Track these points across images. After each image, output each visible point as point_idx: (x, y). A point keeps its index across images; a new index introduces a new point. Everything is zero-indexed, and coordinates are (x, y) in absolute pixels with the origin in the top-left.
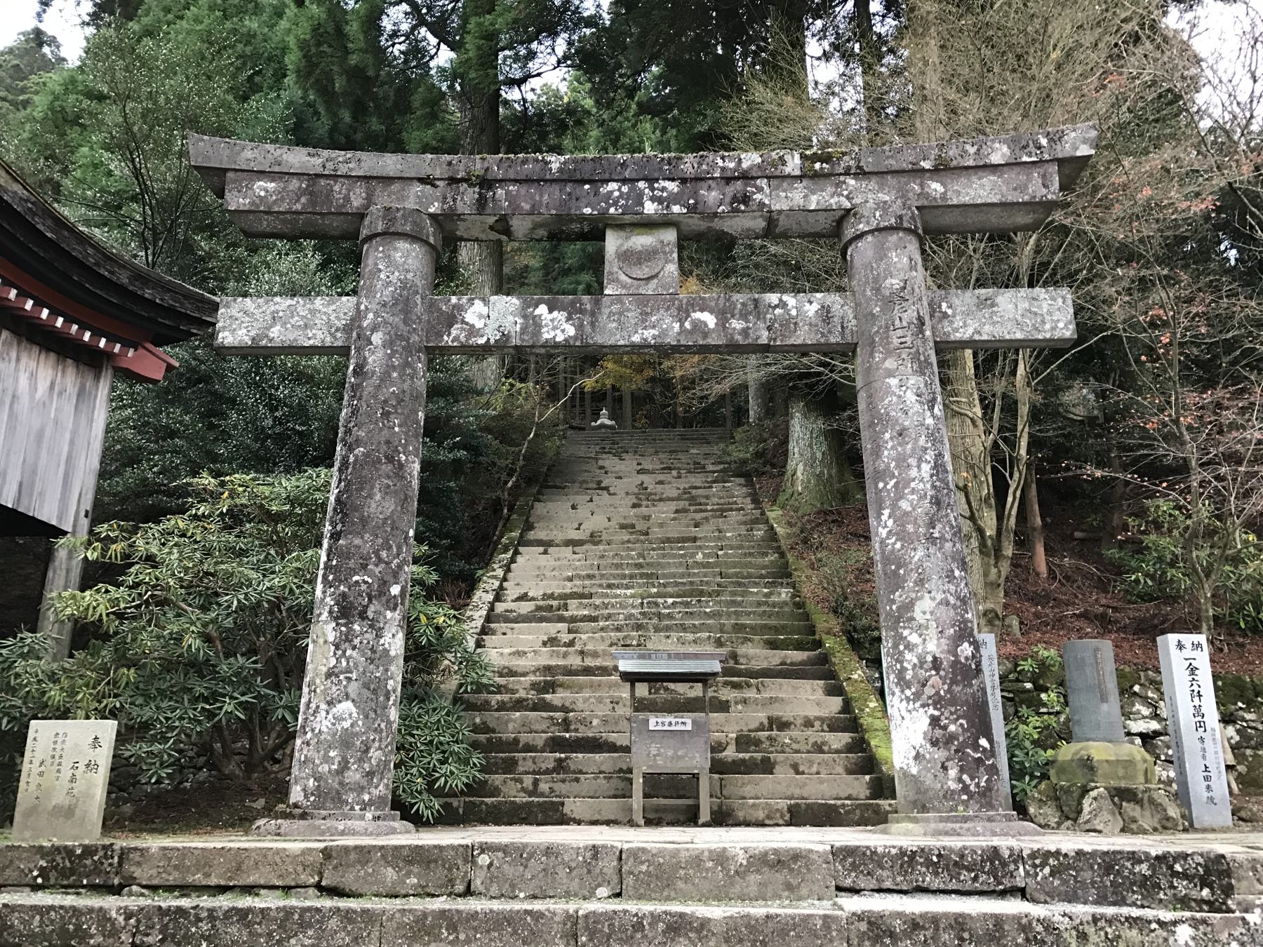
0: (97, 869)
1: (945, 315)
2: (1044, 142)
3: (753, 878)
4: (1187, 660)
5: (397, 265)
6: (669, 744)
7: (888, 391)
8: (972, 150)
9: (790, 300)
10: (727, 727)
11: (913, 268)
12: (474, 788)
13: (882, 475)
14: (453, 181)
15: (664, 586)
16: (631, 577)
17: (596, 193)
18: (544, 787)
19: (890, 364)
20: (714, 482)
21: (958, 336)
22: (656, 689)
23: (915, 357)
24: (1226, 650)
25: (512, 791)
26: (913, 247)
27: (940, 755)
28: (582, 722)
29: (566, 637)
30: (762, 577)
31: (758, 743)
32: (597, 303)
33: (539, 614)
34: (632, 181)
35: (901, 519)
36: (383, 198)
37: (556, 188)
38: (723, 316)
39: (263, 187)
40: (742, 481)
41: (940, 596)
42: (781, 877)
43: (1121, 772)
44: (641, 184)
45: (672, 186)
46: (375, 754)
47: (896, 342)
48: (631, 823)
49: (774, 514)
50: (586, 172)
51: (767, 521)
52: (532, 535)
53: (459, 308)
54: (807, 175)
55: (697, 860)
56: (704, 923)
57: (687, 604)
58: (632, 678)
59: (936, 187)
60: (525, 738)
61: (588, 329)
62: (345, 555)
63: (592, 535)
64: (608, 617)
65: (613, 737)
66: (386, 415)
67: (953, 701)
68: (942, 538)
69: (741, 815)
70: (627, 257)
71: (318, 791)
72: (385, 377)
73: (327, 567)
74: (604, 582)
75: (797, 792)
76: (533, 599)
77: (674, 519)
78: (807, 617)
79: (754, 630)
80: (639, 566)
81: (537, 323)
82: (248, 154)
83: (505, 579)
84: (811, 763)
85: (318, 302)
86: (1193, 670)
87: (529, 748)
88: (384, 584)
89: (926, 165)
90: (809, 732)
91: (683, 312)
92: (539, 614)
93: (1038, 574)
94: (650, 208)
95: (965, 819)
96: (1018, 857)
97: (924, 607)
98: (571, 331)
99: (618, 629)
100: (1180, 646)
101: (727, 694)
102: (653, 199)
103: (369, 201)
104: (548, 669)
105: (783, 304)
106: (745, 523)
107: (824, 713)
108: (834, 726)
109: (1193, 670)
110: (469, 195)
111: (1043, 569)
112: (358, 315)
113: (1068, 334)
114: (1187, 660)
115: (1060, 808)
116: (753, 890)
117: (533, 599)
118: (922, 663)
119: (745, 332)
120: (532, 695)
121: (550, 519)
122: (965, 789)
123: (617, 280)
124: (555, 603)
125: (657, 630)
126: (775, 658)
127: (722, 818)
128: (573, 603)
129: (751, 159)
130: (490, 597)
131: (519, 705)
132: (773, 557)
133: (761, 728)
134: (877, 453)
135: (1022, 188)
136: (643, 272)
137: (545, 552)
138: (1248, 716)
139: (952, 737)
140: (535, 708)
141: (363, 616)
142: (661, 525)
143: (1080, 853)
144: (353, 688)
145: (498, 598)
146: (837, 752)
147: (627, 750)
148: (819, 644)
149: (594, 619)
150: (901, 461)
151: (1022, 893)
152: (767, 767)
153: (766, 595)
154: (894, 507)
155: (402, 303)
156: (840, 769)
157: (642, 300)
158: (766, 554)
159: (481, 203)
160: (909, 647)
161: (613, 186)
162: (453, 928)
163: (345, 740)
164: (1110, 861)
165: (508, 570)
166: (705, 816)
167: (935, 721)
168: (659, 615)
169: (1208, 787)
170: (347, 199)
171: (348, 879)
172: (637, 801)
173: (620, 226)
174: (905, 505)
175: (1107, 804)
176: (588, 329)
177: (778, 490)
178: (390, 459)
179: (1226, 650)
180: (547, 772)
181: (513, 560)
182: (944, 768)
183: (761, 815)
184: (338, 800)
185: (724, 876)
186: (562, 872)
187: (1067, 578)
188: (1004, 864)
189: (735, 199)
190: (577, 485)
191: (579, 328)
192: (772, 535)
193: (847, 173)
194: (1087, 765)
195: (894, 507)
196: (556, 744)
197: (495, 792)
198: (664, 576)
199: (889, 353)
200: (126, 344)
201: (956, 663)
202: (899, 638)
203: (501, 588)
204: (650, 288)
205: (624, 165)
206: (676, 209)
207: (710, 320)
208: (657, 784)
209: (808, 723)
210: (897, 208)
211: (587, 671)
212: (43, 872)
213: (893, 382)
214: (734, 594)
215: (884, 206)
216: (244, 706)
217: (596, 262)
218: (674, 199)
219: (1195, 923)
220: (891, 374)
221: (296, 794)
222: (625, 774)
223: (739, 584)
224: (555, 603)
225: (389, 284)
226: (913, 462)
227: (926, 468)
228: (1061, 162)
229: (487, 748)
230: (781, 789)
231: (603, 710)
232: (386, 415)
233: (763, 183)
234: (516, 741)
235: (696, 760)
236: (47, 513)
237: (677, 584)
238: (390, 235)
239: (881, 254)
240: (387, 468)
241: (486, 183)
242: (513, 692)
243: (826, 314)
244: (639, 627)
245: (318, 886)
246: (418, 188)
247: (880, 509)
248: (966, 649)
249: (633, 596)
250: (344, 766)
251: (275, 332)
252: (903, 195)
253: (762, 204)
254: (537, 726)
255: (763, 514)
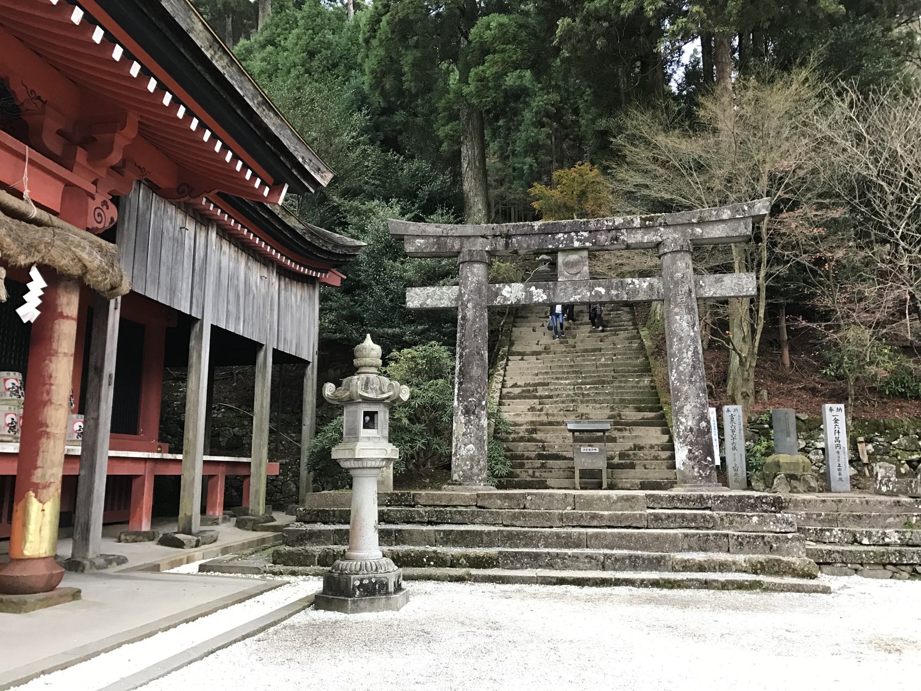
0: (406, 500)
1: (701, 286)
2: (746, 208)
3: (619, 504)
4: (835, 419)
5: (475, 274)
6: (590, 456)
7: (676, 322)
8: (714, 213)
9: (636, 281)
10: (615, 449)
11: (688, 268)
12: (510, 475)
13: (674, 355)
14: (495, 236)
15: (585, 378)
16: (568, 373)
17: (554, 239)
18: (537, 474)
19: (677, 310)
20: (612, 310)
21: (707, 295)
22: (583, 437)
23: (687, 307)
24: (876, 405)
25: (524, 476)
26: (688, 259)
27: (692, 463)
28: (551, 447)
29: (539, 407)
30: (635, 372)
31: (629, 456)
32: (555, 285)
33: (524, 394)
34: (569, 233)
35: (680, 373)
36: (467, 246)
37: (537, 237)
38: (608, 289)
39: (419, 242)
40: (627, 309)
41: (693, 404)
42: (628, 504)
43: (792, 467)
44: (573, 234)
45: (586, 234)
46: (482, 463)
47: (679, 300)
48: (575, 489)
49: (644, 333)
50: (549, 229)
51: (640, 338)
52: (514, 349)
53: (500, 289)
54: (643, 227)
55: (600, 498)
56: (602, 516)
57: (596, 388)
58: (573, 431)
59: (698, 230)
60: (526, 454)
61: (552, 296)
62: (465, 391)
63: (545, 348)
64: (558, 396)
65: (564, 454)
66: (475, 336)
67: (697, 444)
68: (696, 381)
69: (620, 486)
70: (567, 265)
71: (464, 476)
72: (474, 321)
73: (458, 395)
74: (554, 376)
75: (645, 476)
76: (520, 386)
77: (589, 337)
78: (657, 394)
79: (630, 402)
80: (572, 366)
81: (531, 295)
82: (412, 228)
83: (505, 376)
84: (651, 464)
85: (444, 288)
86: (836, 421)
87: (528, 458)
88: (480, 401)
89: (694, 221)
90: (652, 451)
91: (591, 288)
92: (524, 394)
93: (784, 365)
94: (576, 244)
95: (700, 486)
96: (709, 498)
97: (687, 408)
98: (545, 297)
99: (563, 402)
100: (831, 410)
101: (616, 434)
102: (577, 240)
103: (462, 247)
104: (532, 423)
105: (633, 283)
106: (628, 339)
107: (658, 442)
108: (664, 448)
109: (836, 421)
110: (502, 242)
111: (787, 362)
112: (460, 295)
113: (753, 293)
114: (835, 419)
115: (765, 483)
116: (619, 508)
117: (520, 386)
118: (686, 429)
119: (617, 295)
120: (526, 435)
121: (522, 338)
122: (701, 475)
123: (563, 275)
124: (531, 388)
125: (582, 402)
126: (639, 416)
127: (611, 487)
128: (540, 388)
129: (619, 220)
130: (500, 386)
131: (522, 439)
132: (641, 360)
133: (631, 450)
134: (671, 347)
135: (735, 230)
136: (574, 271)
137: (522, 359)
138: (880, 439)
139: (697, 457)
140: (529, 441)
141: (474, 413)
142: (582, 341)
143: (730, 496)
144: (473, 439)
145: (503, 386)
146: (664, 459)
147: (572, 459)
148: (661, 408)
149: (550, 397)
150: (680, 350)
151: (710, 509)
152: (632, 466)
153: (638, 382)
154: (677, 369)
155: (478, 290)
156: (664, 467)
157: (574, 283)
158: (638, 358)
159: (507, 245)
160: (682, 423)
161: (560, 235)
162: (524, 517)
163: (472, 458)
164: (740, 499)
165: (505, 371)
166: (605, 486)
167: (690, 451)
168: (583, 394)
169: (840, 474)
170: (453, 246)
171: (486, 504)
172: (577, 479)
173: (563, 250)
174: (681, 368)
175: (785, 481)
176: (552, 296)
177: (647, 317)
178: (478, 353)
179: (876, 405)
180: (538, 468)
181: (507, 365)
182: (693, 468)
183: (629, 486)
184: (471, 479)
185: (610, 503)
186: (555, 502)
187: (800, 367)
188: (704, 499)
189: (612, 239)
190: (534, 315)
191: (548, 296)
192: (642, 347)
193: (660, 225)
194: (778, 465)
195: (677, 369)
196: (540, 456)
197: (518, 476)
198: (585, 372)
199: (676, 306)
200: (322, 271)
201: (699, 430)
202: (678, 420)
203: (504, 381)
204: (577, 278)
205: (565, 226)
206: (587, 244)
207: (602, 290)
208: (584, 473)
209: (652, 447)
210: (680, 242)
211: (550, 424)
212: (389, 501)
213: (678, 317)
214: (621, 382)
215: (675, 241)
216: (423, 444)
217: (553, 264)
218: (586, 239)
219: (759, 516)
220: (677, 314)
221: (455, 477)
222: (572, 469)
223: (623, 376)
224: (531, 388)
225: (472, 283)
226: (685, 351)
227: (690, 353)
228: (753, 217)
229: (513, 457)
230: (638, 475)
231: (559, 441)
232: (475, 336)
233: (624, 231)
234: (523, 455)
235: (601, 464)
236: (304, 356)
237: (591, 377)
238: (472, 262)
239: (674, 262)
240: (477, 357)
241: (508, 236)
242: (518, 433)
243: (651, 286)
244: (573, 401)
245: (476, 506)
246: (481, 240)
247: (672, 369)
248: (704, 424)
249: (569, 384)
250: (472, 467)
251: (429, 302)
252: (684, 234)
253: (624, 241)
254: (529, 449)
255: (638, 333)
